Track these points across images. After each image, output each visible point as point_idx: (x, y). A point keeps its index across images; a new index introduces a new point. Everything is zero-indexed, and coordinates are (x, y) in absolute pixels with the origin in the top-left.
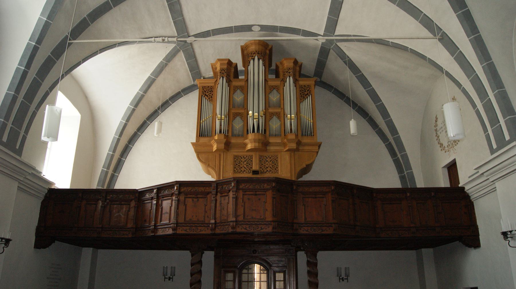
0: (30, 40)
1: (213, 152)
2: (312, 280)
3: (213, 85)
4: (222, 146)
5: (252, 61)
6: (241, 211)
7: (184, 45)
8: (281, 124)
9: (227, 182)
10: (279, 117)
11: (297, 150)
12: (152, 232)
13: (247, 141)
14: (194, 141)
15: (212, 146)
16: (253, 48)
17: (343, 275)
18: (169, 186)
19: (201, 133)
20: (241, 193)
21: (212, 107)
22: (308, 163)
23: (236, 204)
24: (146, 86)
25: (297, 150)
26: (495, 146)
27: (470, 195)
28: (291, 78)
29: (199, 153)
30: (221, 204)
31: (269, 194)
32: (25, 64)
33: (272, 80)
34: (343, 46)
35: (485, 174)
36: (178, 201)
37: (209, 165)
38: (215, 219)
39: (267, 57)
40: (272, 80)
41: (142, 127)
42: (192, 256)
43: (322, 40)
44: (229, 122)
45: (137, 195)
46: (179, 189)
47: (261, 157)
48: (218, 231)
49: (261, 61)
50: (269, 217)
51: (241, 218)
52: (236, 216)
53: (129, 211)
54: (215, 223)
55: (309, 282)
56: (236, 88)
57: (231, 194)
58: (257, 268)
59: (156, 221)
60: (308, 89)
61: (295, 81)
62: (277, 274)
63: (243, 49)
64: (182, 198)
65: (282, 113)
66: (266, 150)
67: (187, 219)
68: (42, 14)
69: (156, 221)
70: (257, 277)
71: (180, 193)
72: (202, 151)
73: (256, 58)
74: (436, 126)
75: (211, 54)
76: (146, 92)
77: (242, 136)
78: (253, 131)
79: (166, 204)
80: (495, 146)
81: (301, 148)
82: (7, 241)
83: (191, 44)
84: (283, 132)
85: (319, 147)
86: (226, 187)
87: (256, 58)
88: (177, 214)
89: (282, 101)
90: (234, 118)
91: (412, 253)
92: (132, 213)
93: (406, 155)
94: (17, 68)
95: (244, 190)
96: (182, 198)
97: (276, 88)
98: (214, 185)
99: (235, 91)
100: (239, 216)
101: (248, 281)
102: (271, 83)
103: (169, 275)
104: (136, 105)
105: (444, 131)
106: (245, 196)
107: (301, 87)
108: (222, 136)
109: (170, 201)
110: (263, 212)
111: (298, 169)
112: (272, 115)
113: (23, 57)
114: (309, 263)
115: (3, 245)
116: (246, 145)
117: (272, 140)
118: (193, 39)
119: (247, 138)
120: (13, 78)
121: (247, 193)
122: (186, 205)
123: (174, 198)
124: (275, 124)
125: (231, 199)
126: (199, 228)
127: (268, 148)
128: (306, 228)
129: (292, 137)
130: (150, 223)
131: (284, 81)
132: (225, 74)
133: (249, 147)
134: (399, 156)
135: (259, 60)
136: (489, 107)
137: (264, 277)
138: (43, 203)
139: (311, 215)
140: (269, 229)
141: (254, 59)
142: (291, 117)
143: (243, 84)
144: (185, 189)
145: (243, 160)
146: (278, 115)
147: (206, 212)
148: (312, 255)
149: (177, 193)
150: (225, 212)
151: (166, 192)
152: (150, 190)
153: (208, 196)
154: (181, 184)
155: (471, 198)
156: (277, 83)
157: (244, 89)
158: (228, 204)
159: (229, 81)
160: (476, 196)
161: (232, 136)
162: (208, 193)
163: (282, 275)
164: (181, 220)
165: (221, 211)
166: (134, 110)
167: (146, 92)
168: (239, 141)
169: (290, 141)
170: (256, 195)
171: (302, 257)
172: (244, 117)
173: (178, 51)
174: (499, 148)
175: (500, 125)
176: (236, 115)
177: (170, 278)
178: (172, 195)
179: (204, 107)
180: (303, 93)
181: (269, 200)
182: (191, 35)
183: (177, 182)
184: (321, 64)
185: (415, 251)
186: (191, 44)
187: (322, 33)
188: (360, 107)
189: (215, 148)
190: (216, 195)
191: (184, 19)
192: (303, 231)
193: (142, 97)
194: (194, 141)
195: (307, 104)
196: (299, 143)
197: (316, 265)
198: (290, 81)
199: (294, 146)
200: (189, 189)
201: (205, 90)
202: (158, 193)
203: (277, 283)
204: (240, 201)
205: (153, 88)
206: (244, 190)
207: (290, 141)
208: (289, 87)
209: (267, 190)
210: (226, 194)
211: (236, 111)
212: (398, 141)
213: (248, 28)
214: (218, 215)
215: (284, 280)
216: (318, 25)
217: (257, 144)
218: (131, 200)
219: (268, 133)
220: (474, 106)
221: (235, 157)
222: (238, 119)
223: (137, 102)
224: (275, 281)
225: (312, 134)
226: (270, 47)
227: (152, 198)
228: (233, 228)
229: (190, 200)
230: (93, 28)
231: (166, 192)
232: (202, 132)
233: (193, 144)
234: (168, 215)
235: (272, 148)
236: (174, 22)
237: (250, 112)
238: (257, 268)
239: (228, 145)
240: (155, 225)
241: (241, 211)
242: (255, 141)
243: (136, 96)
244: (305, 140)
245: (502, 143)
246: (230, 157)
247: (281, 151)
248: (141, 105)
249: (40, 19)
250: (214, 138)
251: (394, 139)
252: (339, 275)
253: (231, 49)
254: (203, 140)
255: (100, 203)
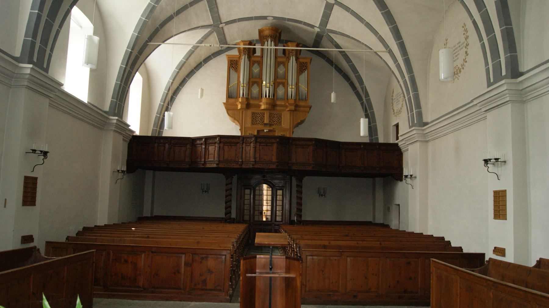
0: (127, 48)
1: (237, 110)
2: (299, 195)
3: (237, 59)
4: (245, 106)
5: (266, 43)
6: (258, 156)
7: (217, 26)
10: (284, 86)
12: (203, 165)
13: (261, 103)
14: (225, 102)
15: (237, 105)
16: (267, 33)
17: (322, 193)
18: (214, 137)
19: (230, 96)
20: (258, 144)
21: (237, 75)
23: (255, 151)
24: (188, 56)
25: (295, 110)
26: (492, 81)
29: (228, 110)
30: (245, 150)
31: (275, 146)
32: (125, 63)
33: (281, 57)
35: (478, 105)
36: (220, 147)
37: (235, 119)
38: (242, 159)
39: (277, 38)
40: (281, 57)
42: (226, 179)
43: (317, 30)
44: (249, 89)
45: (191, 141)
46: (220, 140)
47: (270, 114)
48: (244, 166)
49: (273, 42)
50: (274, 159)
51: (258, 160)
52: (255, 158)
53: (186, 151)
54: (242, 162)
55: (297, 197)
57: (252, 144)
58: (265, 186)
59: (205, 158)
61: (297, 59)
62: (278, 191)
63: (260, 32)
64: (222, 145)
66: (274, 110)
68: (135, 31)
69: (205, 158)
70: (265, 192)
71: (220, 142)
72: (230, 108)
74: (392, 96)
75: (237, 35)
76: (187, 60)
77: (258, 99)
78: (266, 96)
79: (211, 148)
80: (492, 81)
81: (298, 109)
82: (45, 154)
83: (222, 28)
84: (286, 97)
85: (310, 108)
86: (249, 140)
87: (269, 40)
88: (219, 155)
90: (253, 85)
91: (371, 179)
92: (188, 152)
93: (373, 112)
94: (121, 66)
95: (260, 143)
96: (222, 145)
97: (283, 63)
98: (241, 139)
99: (253, 64)
101: (259, 195)
102: (279, 60)
103: (205, 189)
104: (180, 69)
105: (465, 50)
107: (301, 63)
108: (245, 100)
109: (213, 147)
110: (271, 154)
113: (124, 59)
114: (297, 186)
115: (43, 157)
116: (260, 106)
117: (278, 103)
118: (224, 24)
119: (261, 102)
120: (119, 73)
122: (224, 150)
123: (216, 145)
124: (281, 91)
125: (252, 148)
127: (276, 108)
129: (292, 102)
130: (201, 159)
131: (288, 59)
132: (247, 52)
133: (263, 107)
134: (369, 112)
136: (410, 99)
137: (270, 193)
138: (129, 144)
139: (300, 157)
140: (274, 167)
142: (291, 90)
143: (259, 59)
144: (224, 140)
145: (258, 115)
147: (236, 154)
148: (300, 180)
149: (218, 142)
150: (248, 155)
151: (211, 141)
152: (200, 138)
153: (238, 145)
154: (221, 137)
156: (284, 60)
157: (260, 64)
158: (250, 150)
159: (249, 57)
161: (251, 98)
162: (238, 143)
163: (281, 191)
164: (221, 159)
165: (246, 154)
166: (178, 72)
167: (187, 60)
168: (256, 102)
169: (290, 104)
171: (294, 182)
172: (260, 85)
173: (213, 32)
174: (495, 82)
175: (500, 61)
176: (254, 83)
177: (206, 192)
178: (215, 143)
179: (231, 76)
180: (302, 68)
182: (223, 22)
183: (219, 136)
184: (317, 42)
186: (222, 28)
187: (318, 26)
188: (344, 73)
189: (239, 107)
190: (243, 144)
191: (219, 15)
192: (295, 168)
193: (185, 62)
194: (225, 102)
195: (304, 77)
196: (297, 106)
197: (301, 187)
198: (293, 59)
199: (293, 108)
200: (226, 140)
202: (205, 141)
203: (278, 196)
204: (257, 149)
205: (193, 56)
206: (260, 143)
207: (290, 104)
208: (292, 64)
209: (274, 143)
211: (254, 80)
212: (369, 101)
213: (265, 18)
214: (244, 157)
215: (283, 195)
216: (316, 20)
217: (268, 106)
218: (187, 144)
220: (481, 39)
221: (253, 114)
223: (181, 67)
224: (276, 195)
226: (280, 31)
227: (202, 144)
228: (253, 165)
230: (161, 32)
231: (211, 141)
232: (231, 95)
233: (224, 103)
234: (213, 156)
236: (212, 18)
237: (264, 82)
238: (265, 186)
239: (248, 106)
240: (205, 161)
241: (258, 156)
242: (267, 104)
243: (180, 62)
244: (300, 106)
245: (498, 77)
246: (249, 112)
247: (284, 110)
248: (183, 68)
249: (133, 34)
250: (238, 100)
251: (366, 100)
252: (319, 192)
253: (251, 31)
254: (231, 100)
255: (167, 145)
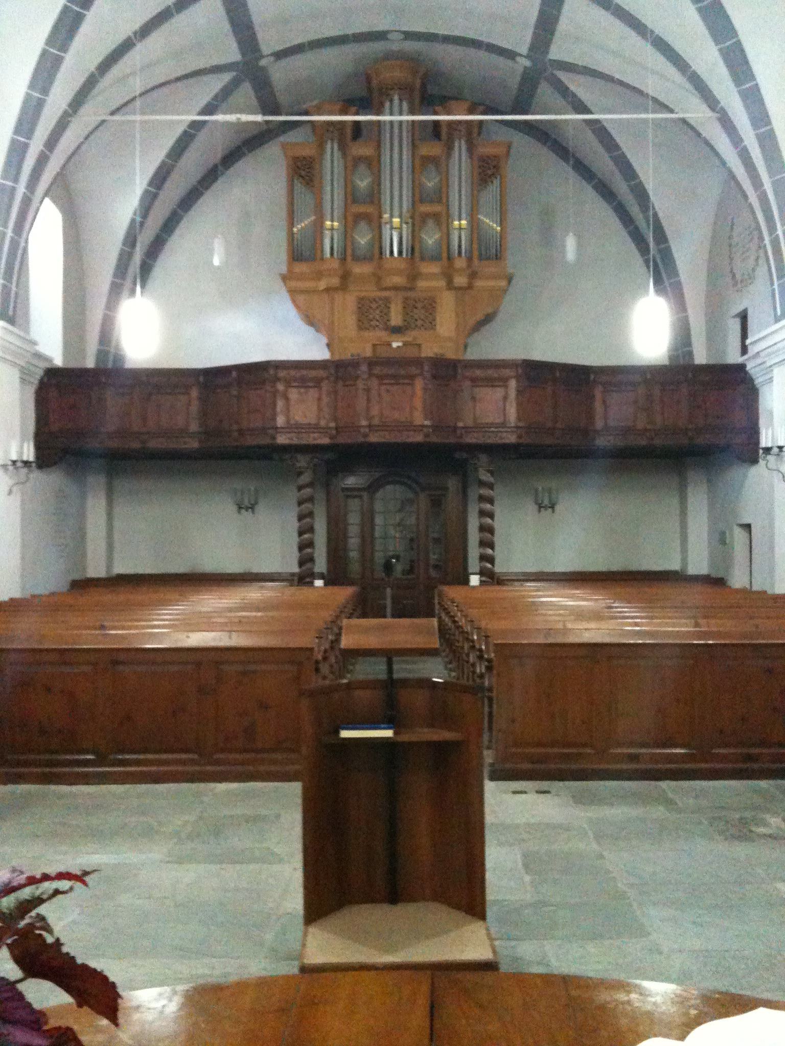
8: (441, 180)
9: (354, 364)
11: (470, 287)
22: (490, 310)
26: (779, 313)
27: (754, 377)
28: (463, 142)
34: (563, 76)
41: (170, 225)
56: (358, 160)
60: (495, 163)
65: (444, 213)
66: (411, 289)
67: (292, 422)
73: (396, 98)
74: (730, 238)
80: (779, 313)
87: (396, 98)
89: (444, 190)
99: (355, 166)
100: (373, 417)
106: (383, 387)
111: (472, 322)
112: (425, 217)
121: (385, 381)
122: (287, 399)
126: (312, 435)
128: (475, 435)
131: (450, 148)
135: (401, 100)
141: (391, 101)
146: (436, 217)
155: (756, 382)
157: (373, 164)
160: (760, 380)
170: (398, 384)
176: (358, 217)
181: (419, 392)
185: (88, 576)
188: (600, 181)
201: (299, 164)
210: (351, 382)
213: (381, 36)
216: (520, 40)
219: (417, 254)
221: (361, 301)
222: (363, 225)
225: (498, 256)
229: (294, 390)
235: (422, 284)
